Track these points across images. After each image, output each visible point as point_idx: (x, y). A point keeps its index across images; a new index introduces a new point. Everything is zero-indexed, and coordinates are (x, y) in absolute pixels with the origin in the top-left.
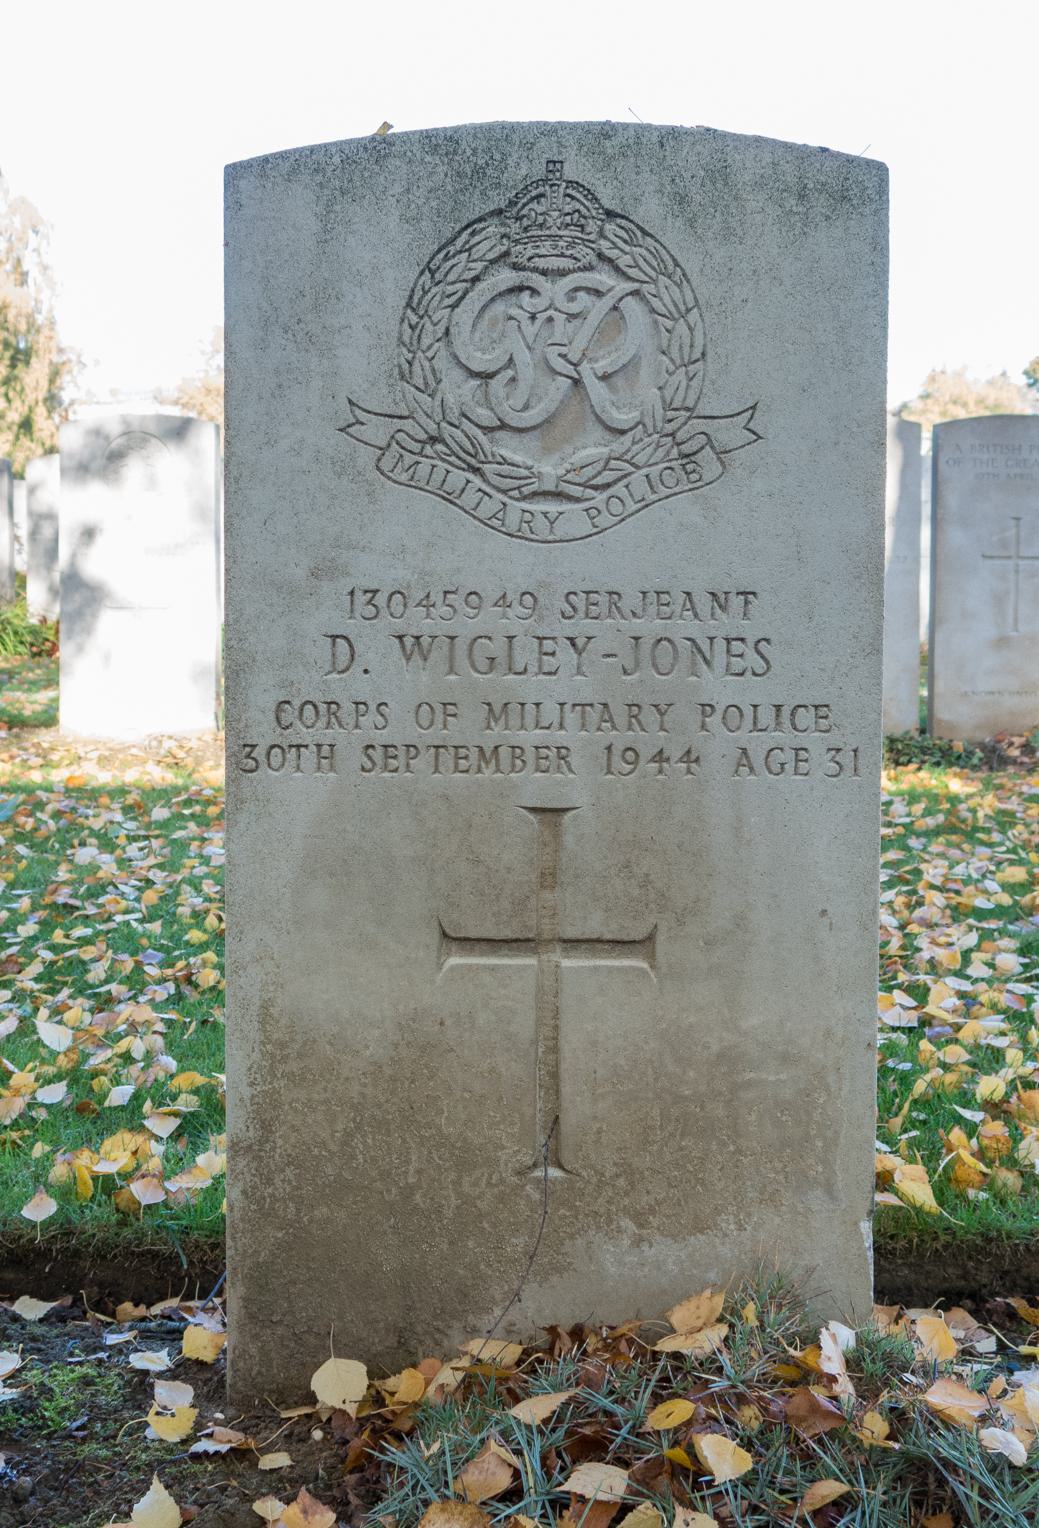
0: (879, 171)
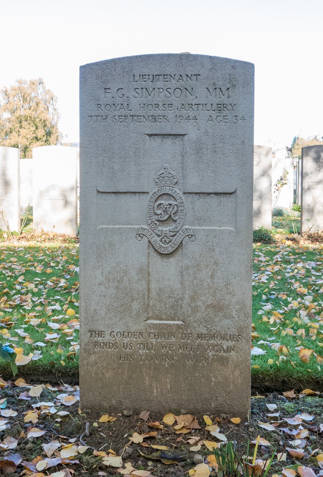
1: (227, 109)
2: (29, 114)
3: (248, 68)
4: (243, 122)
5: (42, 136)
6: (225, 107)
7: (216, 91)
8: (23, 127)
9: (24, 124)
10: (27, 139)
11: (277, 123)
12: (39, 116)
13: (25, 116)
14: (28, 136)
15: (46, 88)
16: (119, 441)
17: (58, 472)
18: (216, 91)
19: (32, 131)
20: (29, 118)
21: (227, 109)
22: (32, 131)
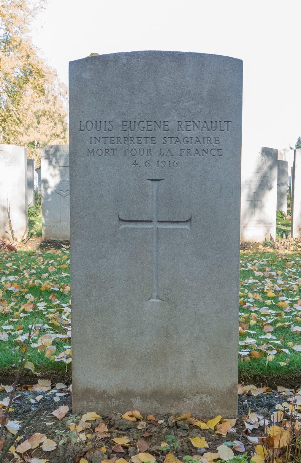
0: (241, 62)
1: (108, 154)
2: (48, 108)
3: (235, 66)
4: (136, 167)
5: (60, 133)
6: (132, 141)
7: (206, 89)
8: (41, 122)
9: (43, 119)
10: (46, 136)
11: (265, 123)
12: (57, 110)
13: (43, 111)
14: (48, 133)
15: (61, 82)
16: (257, 405)
17: (262, 388)
18: (206, 89)
19: (51, 127)
20: (47, 113)
21: (108, 154)
22: (51, 127)
